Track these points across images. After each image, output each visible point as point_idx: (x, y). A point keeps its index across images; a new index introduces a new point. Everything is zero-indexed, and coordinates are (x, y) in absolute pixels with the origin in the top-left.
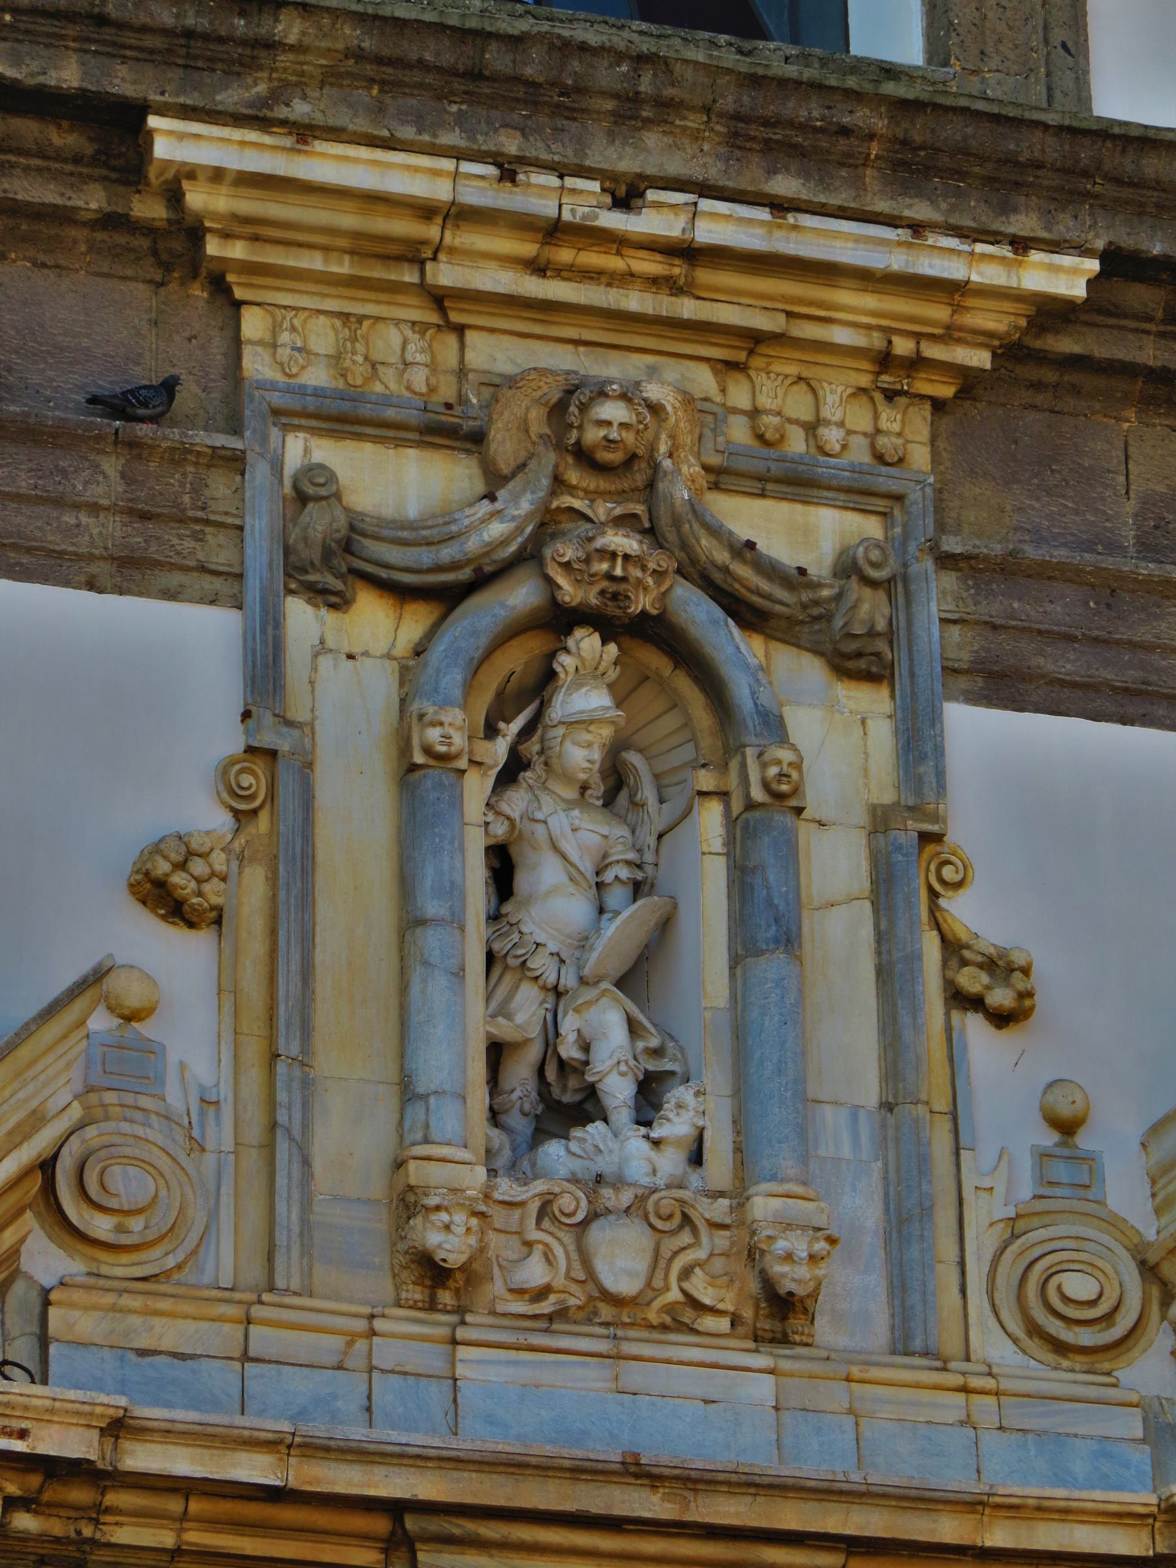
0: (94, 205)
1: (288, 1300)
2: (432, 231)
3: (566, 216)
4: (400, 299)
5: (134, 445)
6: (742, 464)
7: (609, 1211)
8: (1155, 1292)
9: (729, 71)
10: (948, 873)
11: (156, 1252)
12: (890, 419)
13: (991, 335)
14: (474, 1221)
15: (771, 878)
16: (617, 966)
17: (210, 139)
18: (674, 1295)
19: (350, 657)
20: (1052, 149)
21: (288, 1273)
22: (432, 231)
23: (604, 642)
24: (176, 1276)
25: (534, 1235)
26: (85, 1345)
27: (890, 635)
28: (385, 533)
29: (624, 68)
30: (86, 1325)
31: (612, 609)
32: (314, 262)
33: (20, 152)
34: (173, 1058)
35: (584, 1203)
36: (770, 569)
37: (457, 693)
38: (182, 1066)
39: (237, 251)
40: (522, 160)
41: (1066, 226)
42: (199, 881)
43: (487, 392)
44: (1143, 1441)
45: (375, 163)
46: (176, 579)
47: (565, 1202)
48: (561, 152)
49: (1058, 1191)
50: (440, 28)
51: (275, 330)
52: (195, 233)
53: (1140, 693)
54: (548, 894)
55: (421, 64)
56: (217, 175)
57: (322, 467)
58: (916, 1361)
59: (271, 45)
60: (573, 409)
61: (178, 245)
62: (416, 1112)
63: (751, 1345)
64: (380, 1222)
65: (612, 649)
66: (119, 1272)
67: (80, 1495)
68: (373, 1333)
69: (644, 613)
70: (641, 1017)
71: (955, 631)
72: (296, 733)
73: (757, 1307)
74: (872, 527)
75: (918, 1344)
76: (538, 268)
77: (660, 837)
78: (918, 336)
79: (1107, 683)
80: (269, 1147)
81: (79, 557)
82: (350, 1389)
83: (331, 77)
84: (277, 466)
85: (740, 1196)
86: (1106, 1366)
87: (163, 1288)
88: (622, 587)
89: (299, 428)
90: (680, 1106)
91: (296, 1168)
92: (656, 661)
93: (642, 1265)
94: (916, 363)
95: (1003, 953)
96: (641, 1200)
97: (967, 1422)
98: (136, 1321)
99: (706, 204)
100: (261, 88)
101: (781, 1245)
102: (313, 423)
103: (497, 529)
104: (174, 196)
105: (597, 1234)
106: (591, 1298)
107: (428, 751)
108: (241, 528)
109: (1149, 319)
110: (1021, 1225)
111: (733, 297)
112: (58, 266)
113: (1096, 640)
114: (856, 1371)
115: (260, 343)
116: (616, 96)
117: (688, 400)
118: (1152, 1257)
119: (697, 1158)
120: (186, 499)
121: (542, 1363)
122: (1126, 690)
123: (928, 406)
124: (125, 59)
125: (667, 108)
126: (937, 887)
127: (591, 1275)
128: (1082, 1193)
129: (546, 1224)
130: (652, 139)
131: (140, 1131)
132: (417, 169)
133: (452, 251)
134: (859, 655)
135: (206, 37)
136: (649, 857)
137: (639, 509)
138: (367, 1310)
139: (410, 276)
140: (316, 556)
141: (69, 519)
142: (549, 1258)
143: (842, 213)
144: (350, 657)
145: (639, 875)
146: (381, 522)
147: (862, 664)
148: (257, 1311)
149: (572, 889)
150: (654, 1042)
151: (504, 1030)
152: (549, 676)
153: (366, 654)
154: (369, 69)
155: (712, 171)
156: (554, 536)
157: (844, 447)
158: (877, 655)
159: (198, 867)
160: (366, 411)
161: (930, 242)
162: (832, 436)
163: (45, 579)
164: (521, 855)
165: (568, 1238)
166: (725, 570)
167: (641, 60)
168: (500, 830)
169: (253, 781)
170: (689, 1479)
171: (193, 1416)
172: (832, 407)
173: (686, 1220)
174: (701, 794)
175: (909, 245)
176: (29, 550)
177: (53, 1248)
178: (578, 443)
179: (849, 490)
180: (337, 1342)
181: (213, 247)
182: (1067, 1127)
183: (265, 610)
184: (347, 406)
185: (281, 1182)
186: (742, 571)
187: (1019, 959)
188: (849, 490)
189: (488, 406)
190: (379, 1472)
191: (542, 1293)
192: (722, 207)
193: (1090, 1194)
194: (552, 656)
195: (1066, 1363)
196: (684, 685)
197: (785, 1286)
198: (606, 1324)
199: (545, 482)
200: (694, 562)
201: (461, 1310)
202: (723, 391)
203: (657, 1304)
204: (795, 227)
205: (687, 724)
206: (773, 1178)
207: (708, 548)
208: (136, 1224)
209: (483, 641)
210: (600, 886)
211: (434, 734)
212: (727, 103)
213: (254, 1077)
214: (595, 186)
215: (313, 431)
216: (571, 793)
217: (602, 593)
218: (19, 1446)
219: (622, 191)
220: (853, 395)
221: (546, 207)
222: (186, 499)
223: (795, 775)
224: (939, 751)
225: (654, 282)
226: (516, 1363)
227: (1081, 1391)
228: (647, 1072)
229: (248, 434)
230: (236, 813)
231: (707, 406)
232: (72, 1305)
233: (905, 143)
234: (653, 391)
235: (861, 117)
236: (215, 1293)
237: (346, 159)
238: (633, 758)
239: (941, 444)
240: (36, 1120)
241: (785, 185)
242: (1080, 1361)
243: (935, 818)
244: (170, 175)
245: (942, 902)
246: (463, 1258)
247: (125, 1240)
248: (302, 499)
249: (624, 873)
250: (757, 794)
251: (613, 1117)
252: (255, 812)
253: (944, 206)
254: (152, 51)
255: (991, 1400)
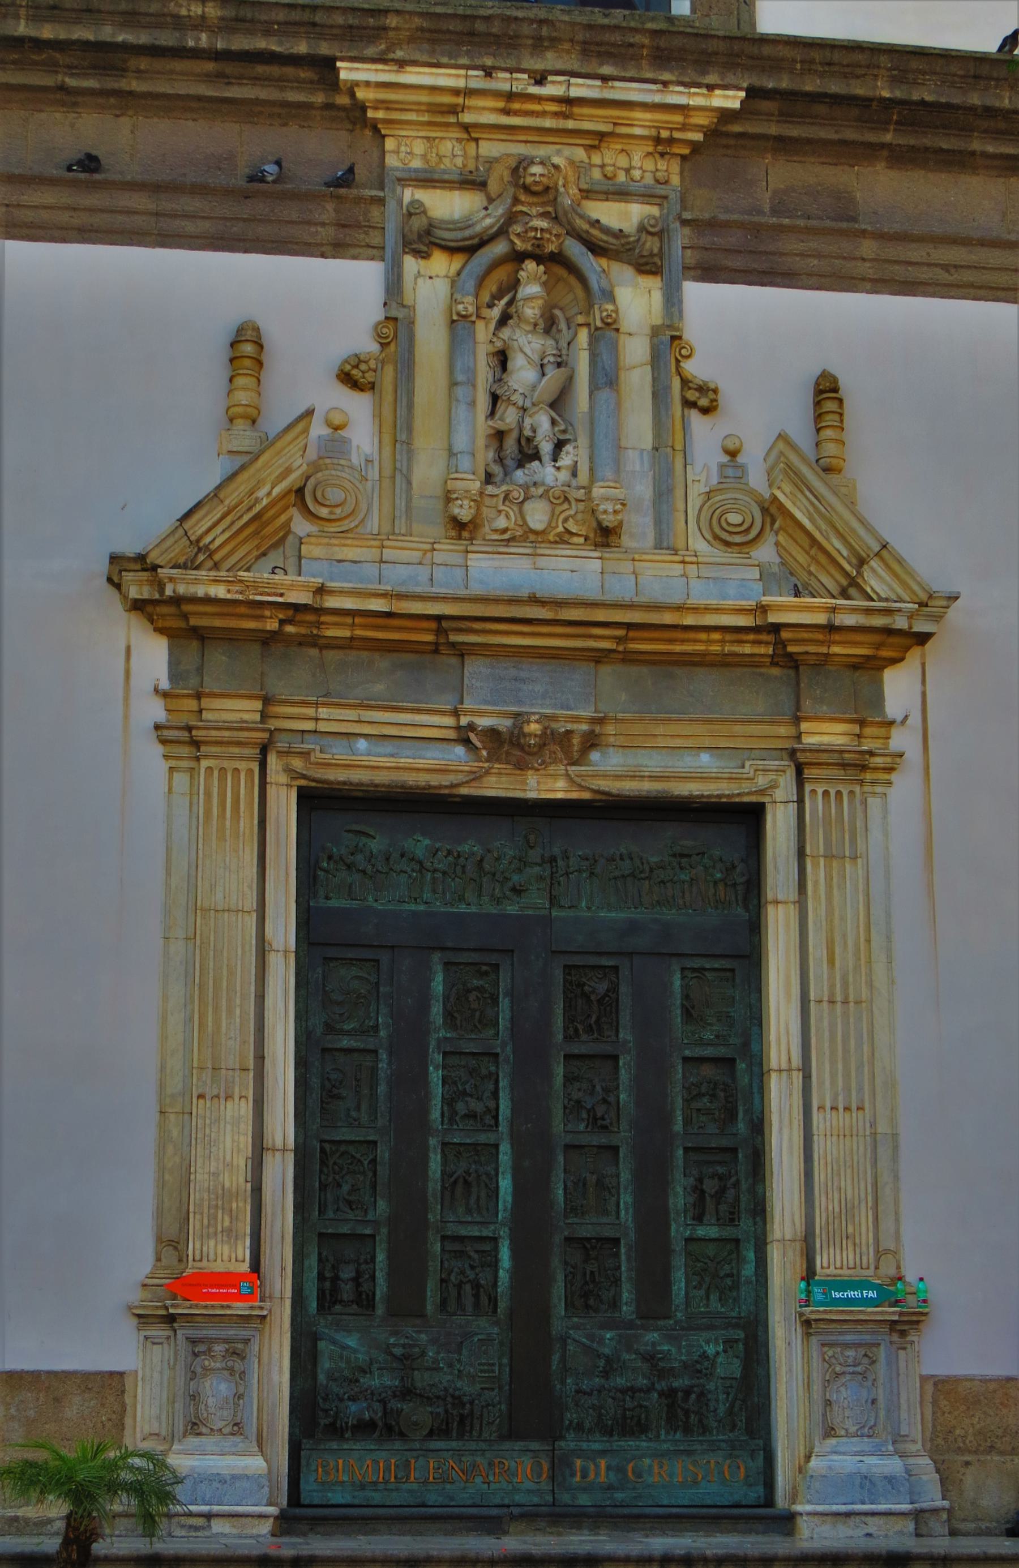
0: (320, 100)
1: (400, 538)
2: (460, 100)
3: (514, 89)
4: (450, 129)
5: (338, 197)
6: (597, 188)
7: (533, 496)
8: (768, 520)
9: (580, 24)
10: (684, 352)
11: (346, 522)
12: (662, 165)
13: (702, 126)
14: (472, 503)
15: (605, 358)
16: (549, 398)
17: (363, 69)
18: (560, 529)
19: (431, 278)
20: (721, 46)
21: (401, 526)
22: (460, 100)
23: (538, 265)
24: (355, 530)
25: (502, 508)
26: (316, 559)
27: (661, 254)
28: (443, 226)
29: (535, 26)
30: (317, 551)
31: (538, 251)
32: (412, 116)
33: (288, 81)
34: (354, 444)
35: (522, 494)
36: (607, 231)
37: (472, 290)
38: (358, 447)
39: (380, 114)
40: (494, 68)
41: (731, 79)
42: (363, 372)
43: (487, 166)
44: (760, 580)
45: (432, 74)
46: (357, 251)
47: (515, 494)
48: (511, 63)
49: (728, 480)
50: (455, 16)
51: (399, 146)
52: (364, 109)
53: (769, 273)
54: (519, 370)
55: (449, 31)
56: (368, 84)
57: (418, 201)
58: (664, 551)
59: (385, 29)
60: (521, 170)
61: (357, 114)
62: (454, 460)
63: (593, 548)
64: (440, 505)
65: (542, 268)
66: (332, 530)
67: (310, 617)
68: (434, 550)
69: (552, 252)
70: (557, 417)
71: (689, 252)
72: (406, 310)
73: (596, 533)
74: (655, 211)
75: (665, 544)
76: (506, 112)
77: (569, 344)
78: (671, 129)
79: (755, 270)
80: (393, 477)
81: (317, 244)
82: (423, 573)
83: (411, 40)
84: (400, 202)
85: (588, 489)
86: (747, 550)
87: (349, 535)
88: (541, 242)
89: (409, 185)
90: (567, 453)
91: (404, 486)
92: (561, 271)
93: (546, 518)
94: (671, 141)
95: (705, 383)
96: (547, 491)
97: (685, 575)
98: (337, 549)
99: (573, 80)
100: (383, 47)
101: (602, 507)
102: (415, 183)
103: (488, 221)
104: (352, 95)
105: (528, 506)
106: (525, 532)
107: (458, 314)
108: (383, 228)
109: (773, 115)
110: (712, 494)
111: (591, 118)
112: (309, 127)
113: (750, 252)
114: (637, 557)
115: (393, 152)
116: (533, 38)
117: (571, 162)
118: (766, 505)
119: (574, 474)
120: (361, 218)
121: (503, 559)
122: (763, 272)
123: (679, 158)
124: (325, 39)
125: (554, 42)
126: (679, 358)
127: (525, 523)
128: (738, 480)
129: (507, 503)
130: (550, 55)
131: (339, 473)
132: (450, 75)
133: (469, 108)
134: (647, 264)
135: (358, 28)
136: (564, 352)
137: (550, 209)
138: (432, 541)
139: (452, 119)
140: (415, 237)
141: (313, 229)
142: (507, 517)
143: (632, 80)
144: (431, 278)
145: (559, 360)
146: (442, 221)
147: (648, 268)
148: (386, 543)
149: (529, 367)
150: (562, 427)
151: (500, 425)
152: (518, 281)
153: (437, 276)
154: (427, 35)
155: (576, 66)
156: (515, 222)
157: (642, 178)
158: (655, 263)
159: (363, 367)
160: (436, 176)
161: (671, 89)
162: (637, 174)
163: (303, 255)
164: (511, 355)
165: (515, 508)
166: (587, 232)
167: (541, 22)
168: (499, 344)
169: (388, 331)
170: (557, 603)
171: (351, 585)
172: (636, 161)
173: (566, 499)
174: (580, 325)
175: (398, 71)
176: (296, 243)
177: (305, 522)
178: (524, 183)
179: (643, 196)
180: (419, 554)
181: (370, 114)
182: (733, 454)
183: (393, 260)
184: (428, 175)
185: (397, 491)
186: (595, 232)
187: (712, 386)
188: (643, 196)
189: (488, 170)
190: (429, 604)
191: (504, 531)
192: (580, 81)
193: (742, 481)
194: (517, 272)
195: (730, 550)
196: (573, 280)
197: (605, 524)
198: (532, 542)
199: (509, 201)
200: (574, 229)
201: (471, 539)
202: (589, 158)
203: (552, 534)
204: (612, 87)
205: (576, 299)
206: (603, 480)
207: (581, 225)
208: (338, 511)
209: (484, 268)
210: (542, 366)
211: (460, 307)
212: (580, 37)
213: (387, 450)
214: (526, 76)
215: (415, 187)
216: (529, 328)
217: (533, 245)
218: (280, 600)
219: (538, 77)
220: (646, 156)
221: (505, 87)
222: (361, 218)
223: (614, 315)
224: (681, 302)
225: (556, 115)
226: (493, 559)
227: (738, 561)
228: (558, 439)
229: (386, 189)
230: (381, 344)
231: (582, 165)
232: (311, 544)
233: (658, 48)
234: (556, 160)
235: (638, 39)
236: (370, 537)
237: (420, 73)
238: (557, 312)
239: (686, 174)
240: (288, 471)
241: (607, 70)
242: (736, 549)
243: (678, 329)
244: (349, 85)
245: (682, 364)
246: (469, 518)
247: (333, 517)
248: (410, 214)
249: (552, 359)
250: (599, 324)
251: (543, 459)
252: (389, 343)
253: (676, 74)
254: (336, 35)
255: (695, 566)
